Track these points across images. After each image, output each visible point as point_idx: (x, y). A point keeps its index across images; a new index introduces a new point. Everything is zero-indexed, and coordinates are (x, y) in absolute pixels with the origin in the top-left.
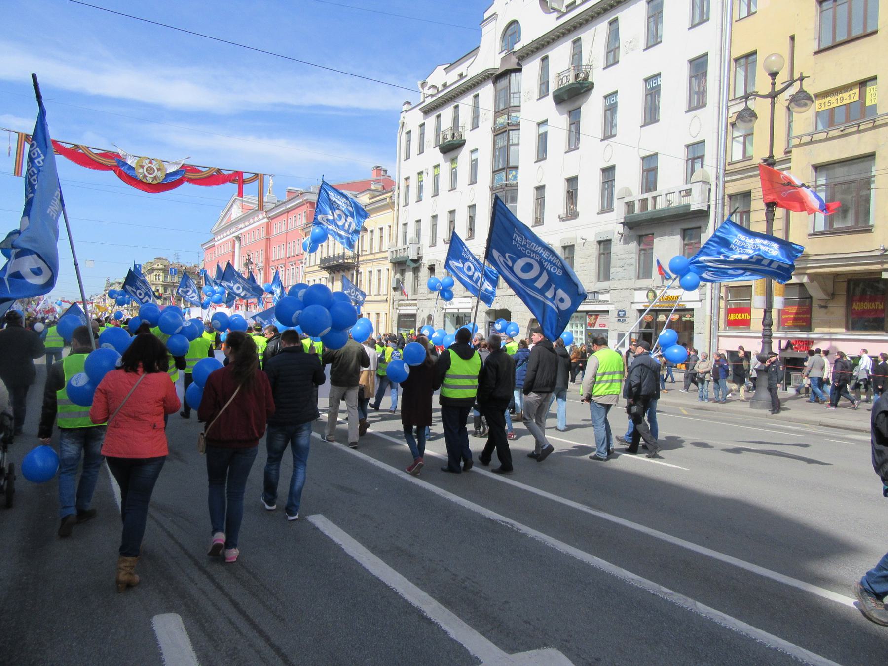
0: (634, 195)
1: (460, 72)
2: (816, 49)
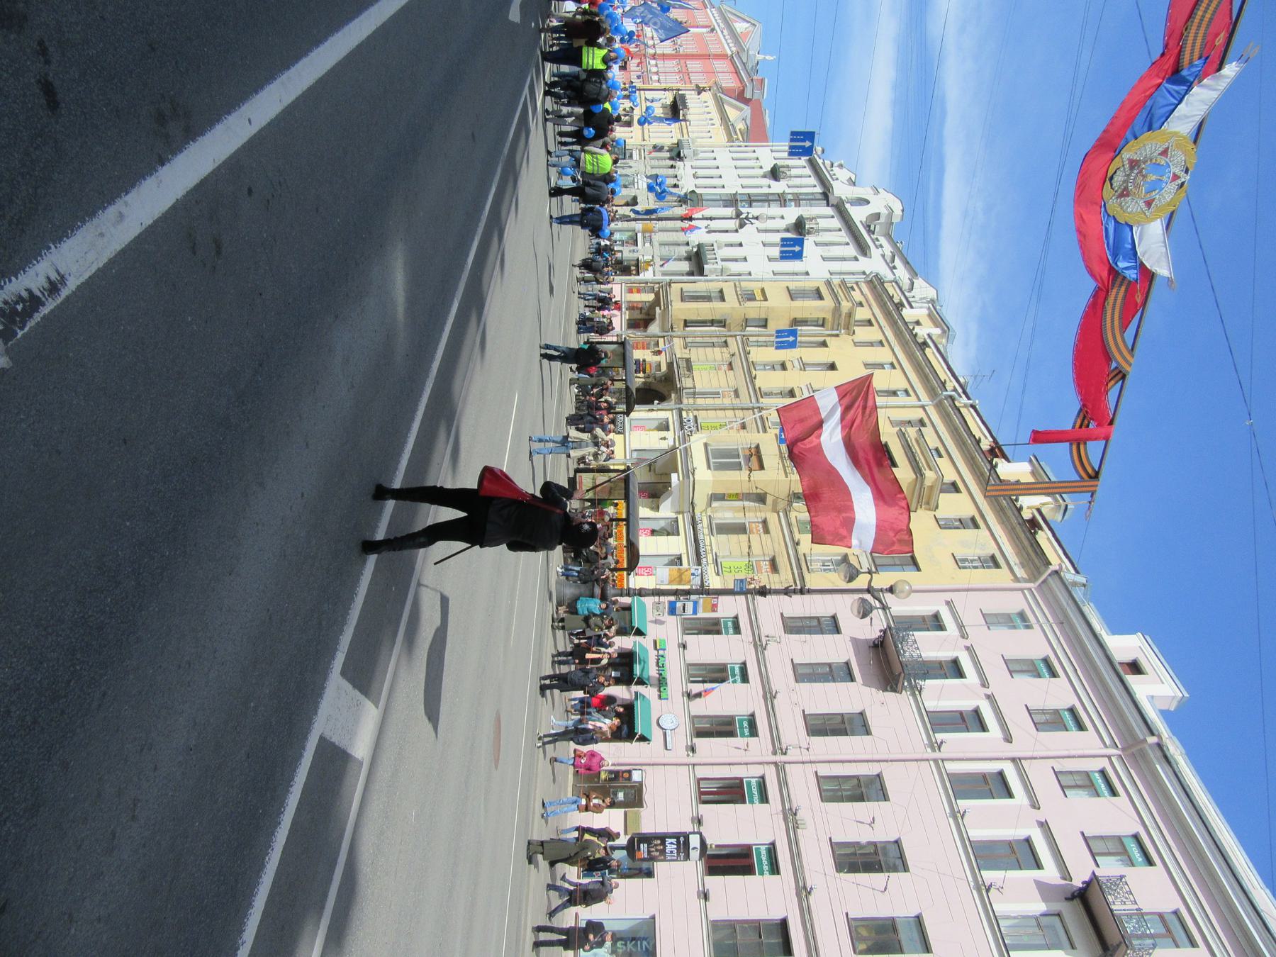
0: (719, 251)
1: (1144, 664)
2: (790, 288)
